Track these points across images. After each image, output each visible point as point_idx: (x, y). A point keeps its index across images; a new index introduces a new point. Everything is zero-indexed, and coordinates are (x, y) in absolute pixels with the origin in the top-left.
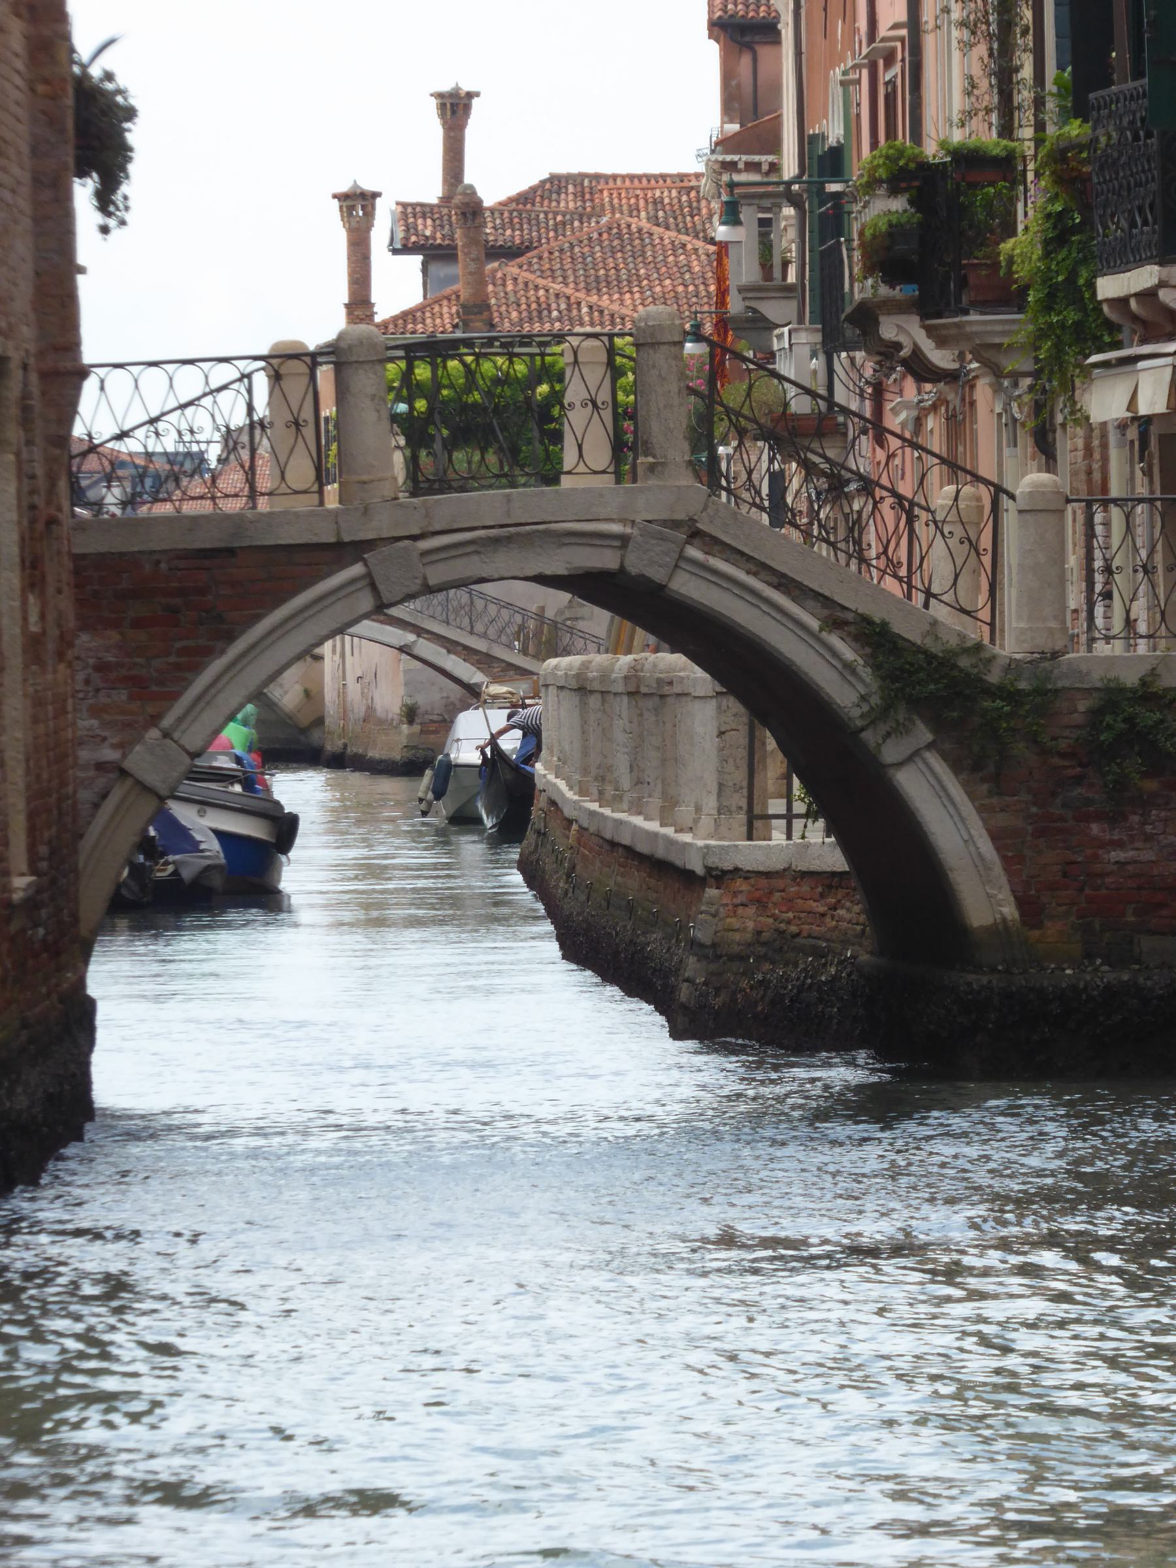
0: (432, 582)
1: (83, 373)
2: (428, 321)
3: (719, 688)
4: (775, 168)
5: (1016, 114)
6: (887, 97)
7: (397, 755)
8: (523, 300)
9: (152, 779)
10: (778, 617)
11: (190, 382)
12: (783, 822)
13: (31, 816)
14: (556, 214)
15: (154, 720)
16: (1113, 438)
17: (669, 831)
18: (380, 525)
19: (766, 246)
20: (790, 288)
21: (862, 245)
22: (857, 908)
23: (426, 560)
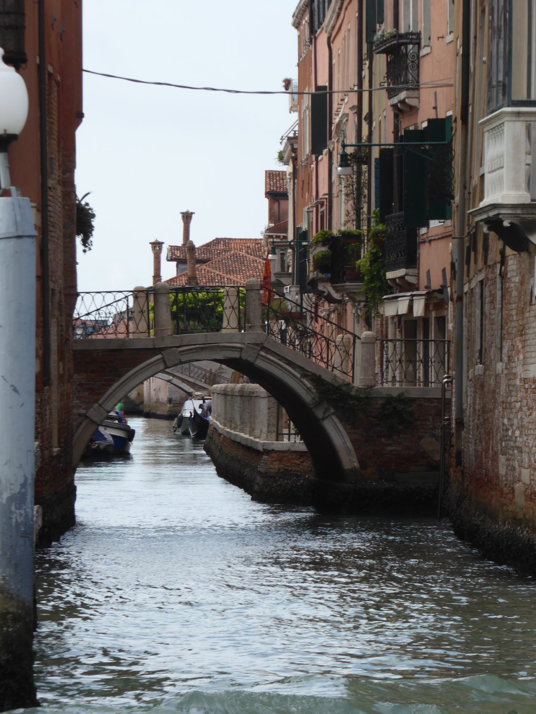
0: (182, 360)
1: (78, 294)
4: (285, 237)
5: (362, 222)
6: (321, 216)
7: (166, 413)
8: (207, 276)
9: (95, 419)
10: (288, 373)
11: (109, 298)
12: (287, 436)
13: (59, 429)
14: (217, 250)
15: (96, 401)
16: (390, 321)
17: (252, 438)
18: (167, 343)
19: (283, 261)
20: (290, 274)
21: (314, 261)
22: (309, 463)
23: (181, 354)
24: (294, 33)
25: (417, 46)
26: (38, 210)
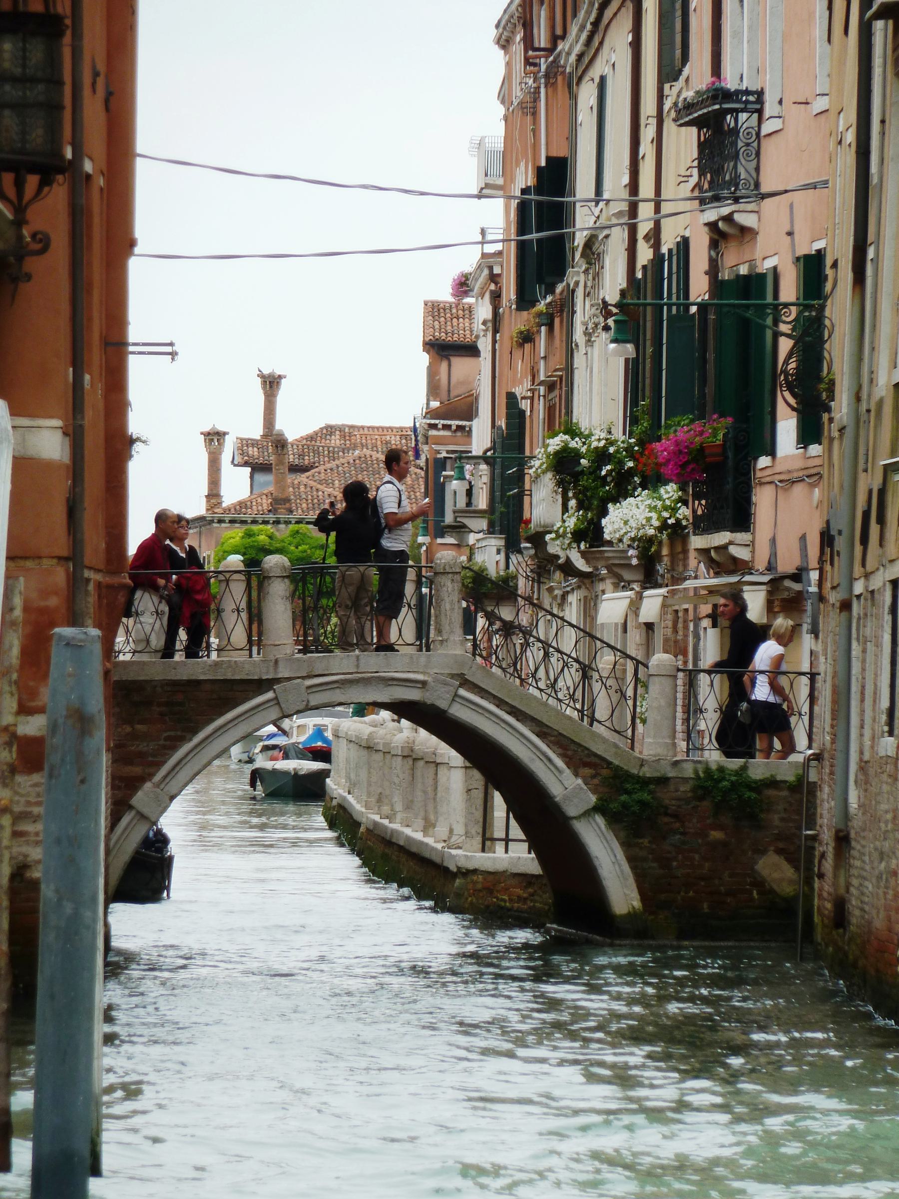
2: (254, 507)
3: (468, 764)
24: (498, 57)
25: (756, 115)
26: (65, 434)
